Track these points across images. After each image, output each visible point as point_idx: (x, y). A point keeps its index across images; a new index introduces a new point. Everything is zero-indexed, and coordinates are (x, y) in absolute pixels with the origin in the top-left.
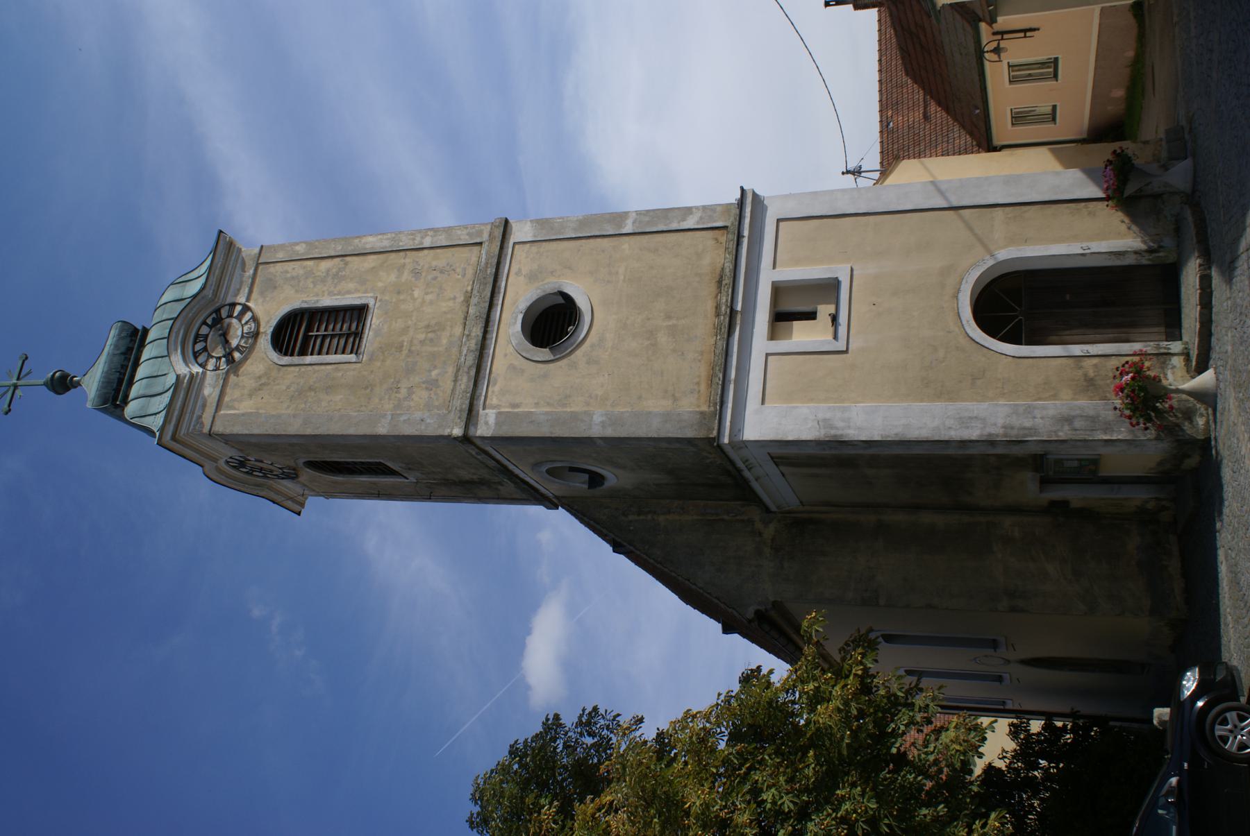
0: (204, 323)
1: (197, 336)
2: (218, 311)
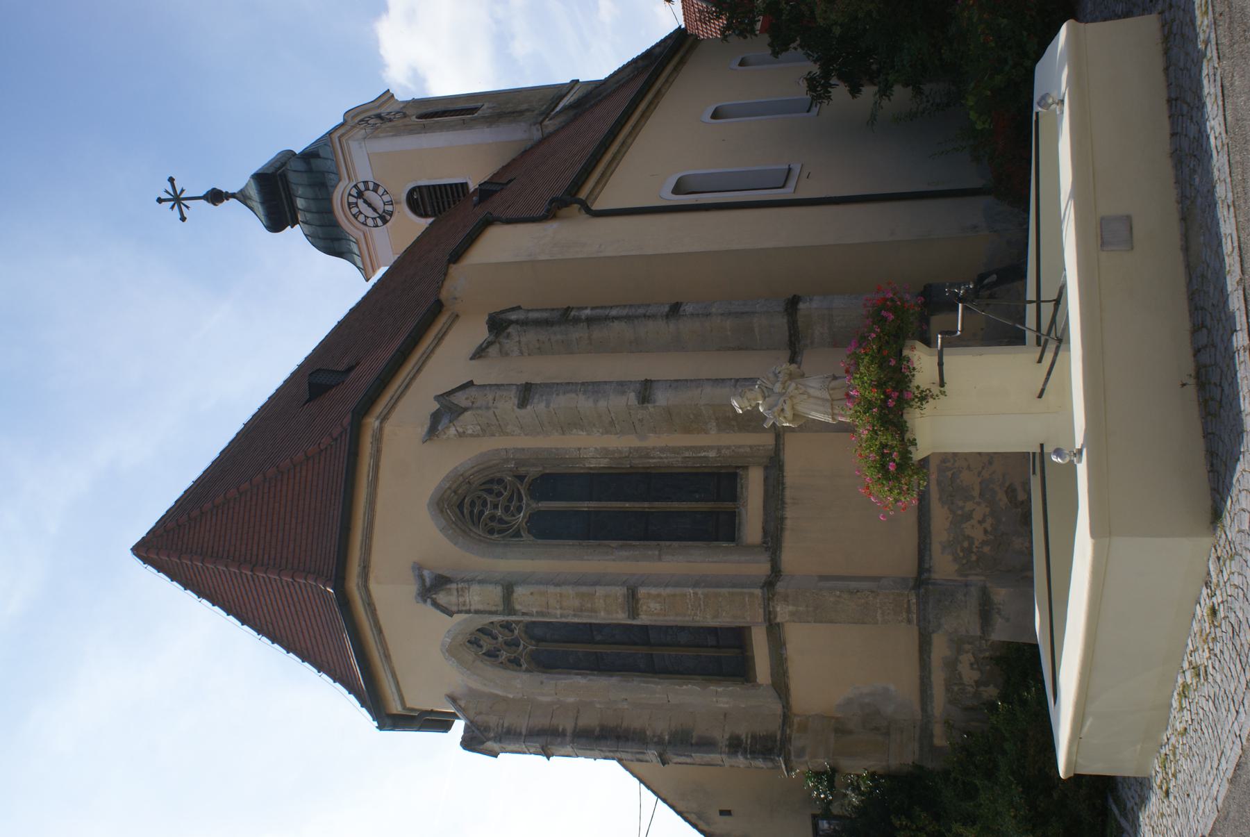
0: (350, 194)
1: (349, 204)
2: (356, 186)
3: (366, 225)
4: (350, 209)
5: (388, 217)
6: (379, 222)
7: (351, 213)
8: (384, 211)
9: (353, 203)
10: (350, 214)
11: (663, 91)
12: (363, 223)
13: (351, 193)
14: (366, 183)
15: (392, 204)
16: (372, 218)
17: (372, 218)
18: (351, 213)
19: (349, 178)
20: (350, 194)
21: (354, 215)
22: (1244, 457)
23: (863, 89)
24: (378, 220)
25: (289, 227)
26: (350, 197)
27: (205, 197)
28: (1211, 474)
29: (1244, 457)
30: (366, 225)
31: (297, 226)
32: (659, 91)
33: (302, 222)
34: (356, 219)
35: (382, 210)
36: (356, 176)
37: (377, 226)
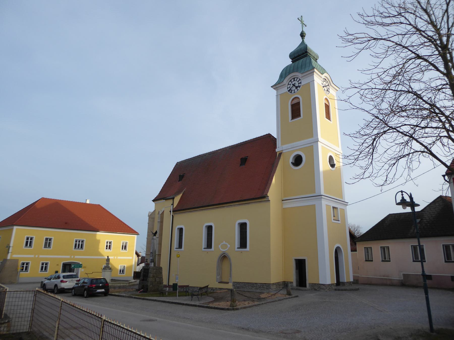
1: (294, 78)
3: (288, 85)
4: (293, 79)
5: (290, 92)
6: (289, 89)
7: (292, 79)
8: (292, 90)
9: (295, 80)
10: (291, 79)
11: (225, 207)
12: (289, 84)
13: (298, 78)
14: (301, 83)
15: (294, 93)
16: (290, 87)
17: (290, 87)
18: (292, 79)
19: (302, 77)
20: (297, 78)
21: (291, 80)
22: (130, 280)
23: (172, 285)
24: (290, 89)
25: (291, 60)
26: (296, 78)
27: (302, 31)
28: (239, 304)
29: (130, 280)
30: (288, 85)
31: (291, 63)
32: (231, 205)
33: (294, 65)
34: (290, 81)
35: (292, 90)
36: (303, 79)
37: (288, 88)
